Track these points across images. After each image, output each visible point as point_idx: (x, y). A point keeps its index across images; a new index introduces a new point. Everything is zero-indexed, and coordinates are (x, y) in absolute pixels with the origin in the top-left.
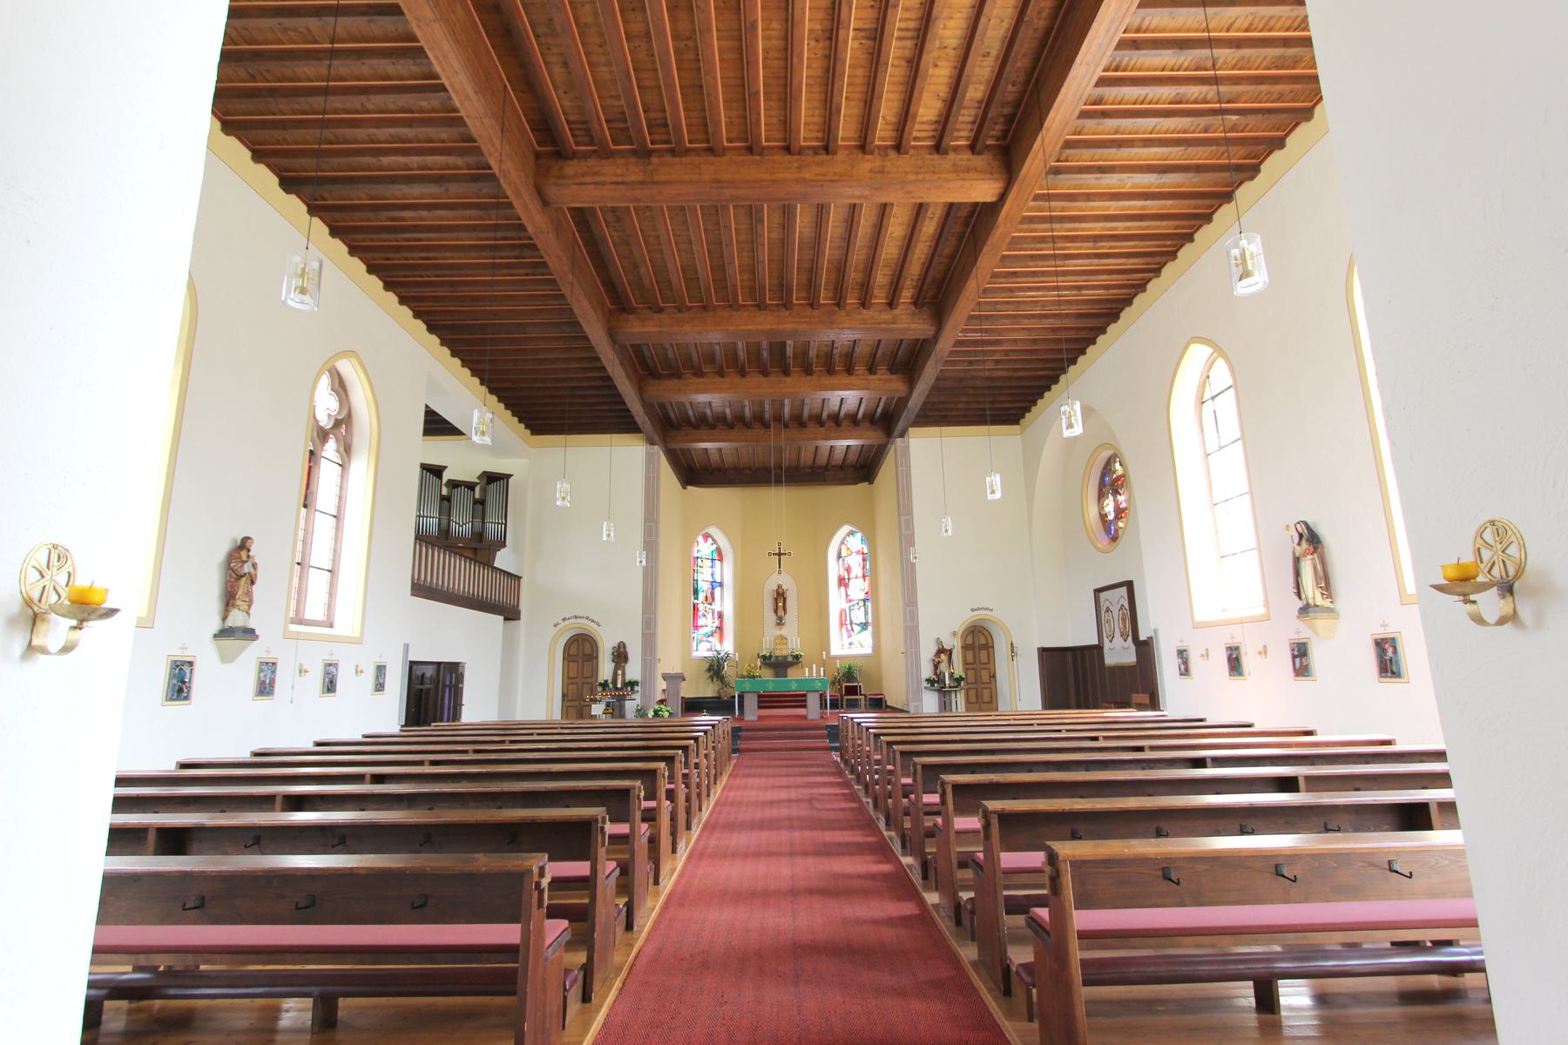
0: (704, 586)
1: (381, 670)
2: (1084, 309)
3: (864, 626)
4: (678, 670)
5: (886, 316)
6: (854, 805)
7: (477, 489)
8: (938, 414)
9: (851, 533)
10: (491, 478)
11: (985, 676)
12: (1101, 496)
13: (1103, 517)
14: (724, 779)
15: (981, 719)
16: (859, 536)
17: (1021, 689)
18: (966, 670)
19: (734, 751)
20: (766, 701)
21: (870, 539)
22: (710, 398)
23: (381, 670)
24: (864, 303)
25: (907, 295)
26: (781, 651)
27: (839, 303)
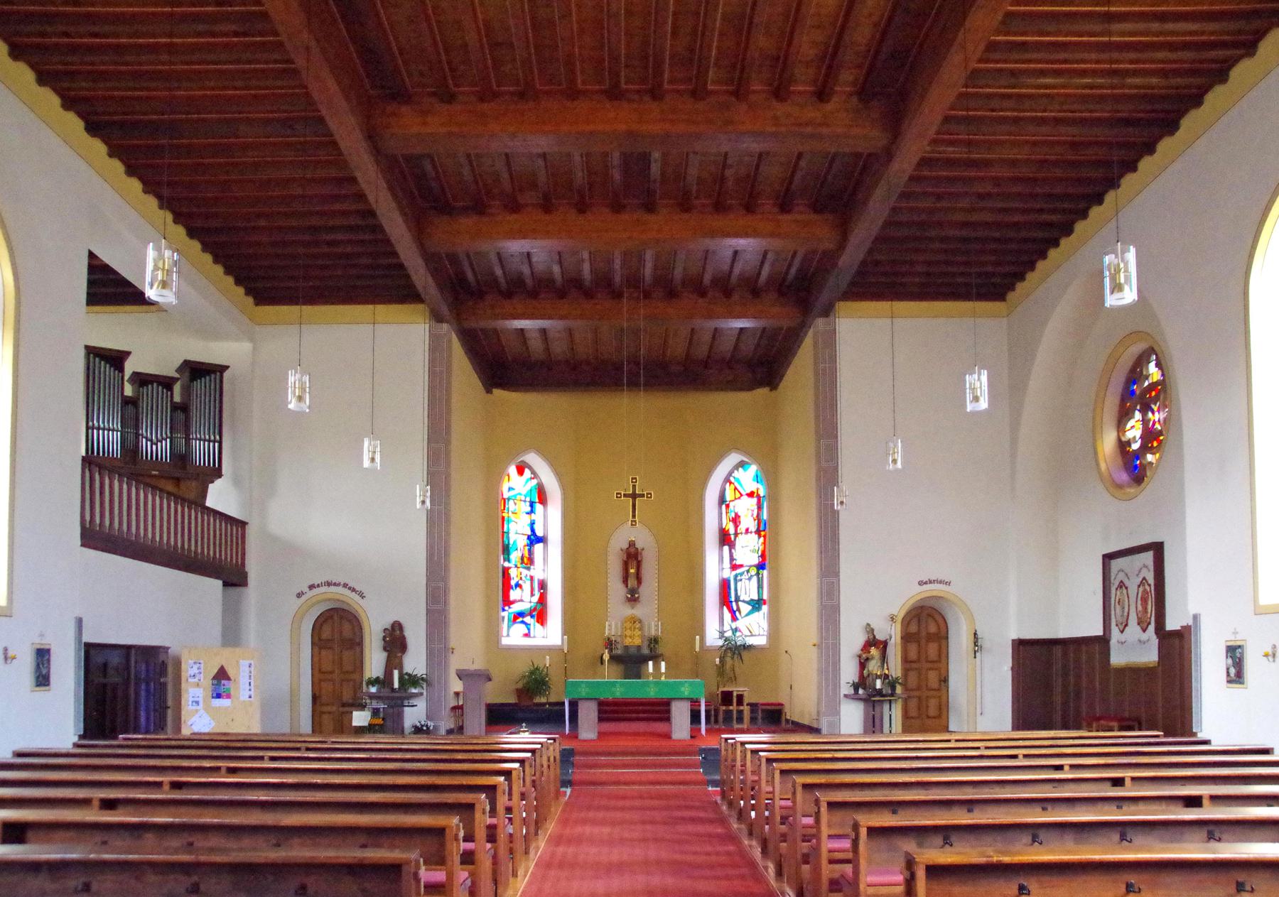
0: (518, 539)
1: (43, 655)
2: (1125, 111)
3: (757, 605)
4: (478, 665)
5: (811, 113)
6: (731, 848)
7: (177, 388)
8: (884, 282)
9: (742, 464)
10: (196, 371)
11: (933, 677)
12: (1123, 416)
13: (1123, 445)
14: (551, 827)
15: (929, 744)
16: (753, 469)
17: (983, 698)
18: (906, 671)
19: (565, 783)
20: (611, 711)
21: (771, 475)
22: (528, 249)
23: (43, 655)
24: (779, 92)
25: (847, 78)
26: (634, 640)
27: (739, 92)
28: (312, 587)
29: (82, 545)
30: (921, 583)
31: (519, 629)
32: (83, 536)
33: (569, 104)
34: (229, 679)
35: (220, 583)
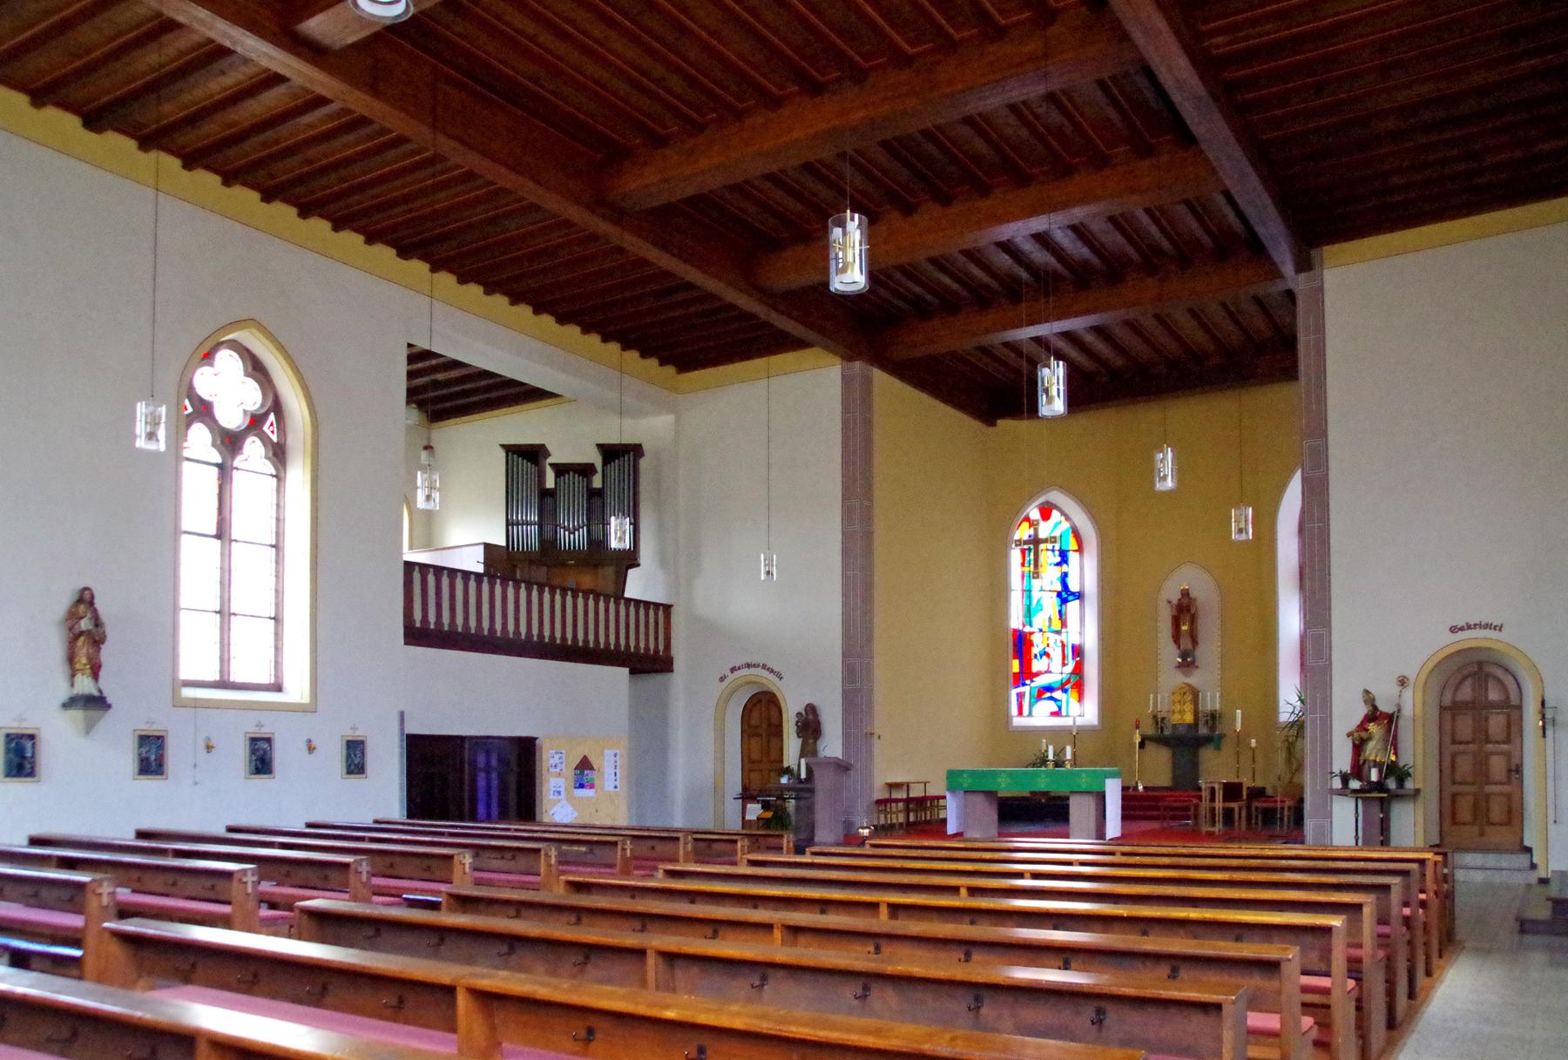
10: (611, 453)
28: (733, 670)
29: (406, 643)
30: (1454, 630)
31: (1046, 706)
32: (407, 635)
33: (771, 115)
34: (592, 768)
35: (626, 670)
